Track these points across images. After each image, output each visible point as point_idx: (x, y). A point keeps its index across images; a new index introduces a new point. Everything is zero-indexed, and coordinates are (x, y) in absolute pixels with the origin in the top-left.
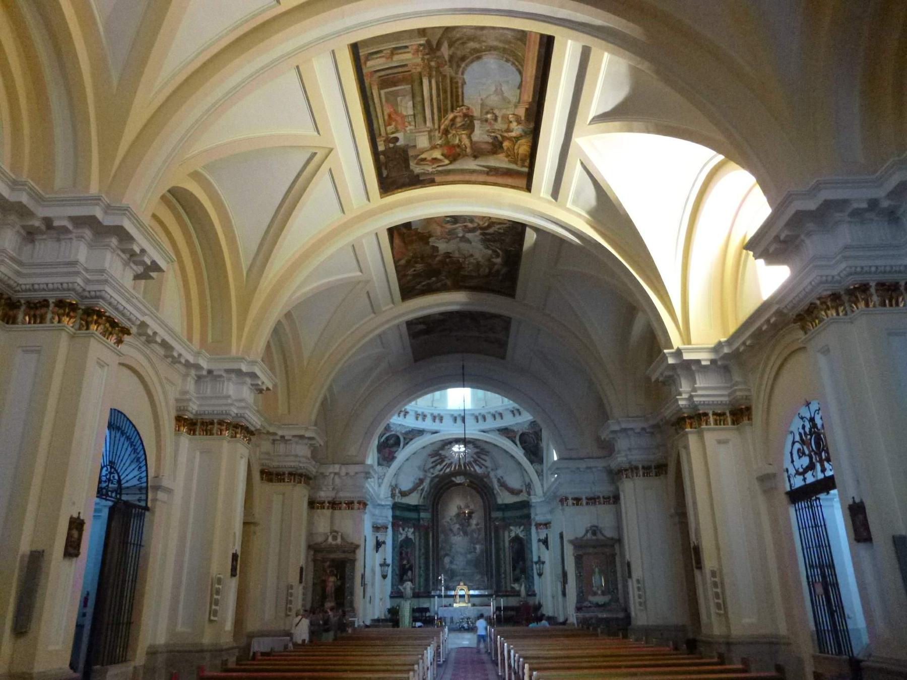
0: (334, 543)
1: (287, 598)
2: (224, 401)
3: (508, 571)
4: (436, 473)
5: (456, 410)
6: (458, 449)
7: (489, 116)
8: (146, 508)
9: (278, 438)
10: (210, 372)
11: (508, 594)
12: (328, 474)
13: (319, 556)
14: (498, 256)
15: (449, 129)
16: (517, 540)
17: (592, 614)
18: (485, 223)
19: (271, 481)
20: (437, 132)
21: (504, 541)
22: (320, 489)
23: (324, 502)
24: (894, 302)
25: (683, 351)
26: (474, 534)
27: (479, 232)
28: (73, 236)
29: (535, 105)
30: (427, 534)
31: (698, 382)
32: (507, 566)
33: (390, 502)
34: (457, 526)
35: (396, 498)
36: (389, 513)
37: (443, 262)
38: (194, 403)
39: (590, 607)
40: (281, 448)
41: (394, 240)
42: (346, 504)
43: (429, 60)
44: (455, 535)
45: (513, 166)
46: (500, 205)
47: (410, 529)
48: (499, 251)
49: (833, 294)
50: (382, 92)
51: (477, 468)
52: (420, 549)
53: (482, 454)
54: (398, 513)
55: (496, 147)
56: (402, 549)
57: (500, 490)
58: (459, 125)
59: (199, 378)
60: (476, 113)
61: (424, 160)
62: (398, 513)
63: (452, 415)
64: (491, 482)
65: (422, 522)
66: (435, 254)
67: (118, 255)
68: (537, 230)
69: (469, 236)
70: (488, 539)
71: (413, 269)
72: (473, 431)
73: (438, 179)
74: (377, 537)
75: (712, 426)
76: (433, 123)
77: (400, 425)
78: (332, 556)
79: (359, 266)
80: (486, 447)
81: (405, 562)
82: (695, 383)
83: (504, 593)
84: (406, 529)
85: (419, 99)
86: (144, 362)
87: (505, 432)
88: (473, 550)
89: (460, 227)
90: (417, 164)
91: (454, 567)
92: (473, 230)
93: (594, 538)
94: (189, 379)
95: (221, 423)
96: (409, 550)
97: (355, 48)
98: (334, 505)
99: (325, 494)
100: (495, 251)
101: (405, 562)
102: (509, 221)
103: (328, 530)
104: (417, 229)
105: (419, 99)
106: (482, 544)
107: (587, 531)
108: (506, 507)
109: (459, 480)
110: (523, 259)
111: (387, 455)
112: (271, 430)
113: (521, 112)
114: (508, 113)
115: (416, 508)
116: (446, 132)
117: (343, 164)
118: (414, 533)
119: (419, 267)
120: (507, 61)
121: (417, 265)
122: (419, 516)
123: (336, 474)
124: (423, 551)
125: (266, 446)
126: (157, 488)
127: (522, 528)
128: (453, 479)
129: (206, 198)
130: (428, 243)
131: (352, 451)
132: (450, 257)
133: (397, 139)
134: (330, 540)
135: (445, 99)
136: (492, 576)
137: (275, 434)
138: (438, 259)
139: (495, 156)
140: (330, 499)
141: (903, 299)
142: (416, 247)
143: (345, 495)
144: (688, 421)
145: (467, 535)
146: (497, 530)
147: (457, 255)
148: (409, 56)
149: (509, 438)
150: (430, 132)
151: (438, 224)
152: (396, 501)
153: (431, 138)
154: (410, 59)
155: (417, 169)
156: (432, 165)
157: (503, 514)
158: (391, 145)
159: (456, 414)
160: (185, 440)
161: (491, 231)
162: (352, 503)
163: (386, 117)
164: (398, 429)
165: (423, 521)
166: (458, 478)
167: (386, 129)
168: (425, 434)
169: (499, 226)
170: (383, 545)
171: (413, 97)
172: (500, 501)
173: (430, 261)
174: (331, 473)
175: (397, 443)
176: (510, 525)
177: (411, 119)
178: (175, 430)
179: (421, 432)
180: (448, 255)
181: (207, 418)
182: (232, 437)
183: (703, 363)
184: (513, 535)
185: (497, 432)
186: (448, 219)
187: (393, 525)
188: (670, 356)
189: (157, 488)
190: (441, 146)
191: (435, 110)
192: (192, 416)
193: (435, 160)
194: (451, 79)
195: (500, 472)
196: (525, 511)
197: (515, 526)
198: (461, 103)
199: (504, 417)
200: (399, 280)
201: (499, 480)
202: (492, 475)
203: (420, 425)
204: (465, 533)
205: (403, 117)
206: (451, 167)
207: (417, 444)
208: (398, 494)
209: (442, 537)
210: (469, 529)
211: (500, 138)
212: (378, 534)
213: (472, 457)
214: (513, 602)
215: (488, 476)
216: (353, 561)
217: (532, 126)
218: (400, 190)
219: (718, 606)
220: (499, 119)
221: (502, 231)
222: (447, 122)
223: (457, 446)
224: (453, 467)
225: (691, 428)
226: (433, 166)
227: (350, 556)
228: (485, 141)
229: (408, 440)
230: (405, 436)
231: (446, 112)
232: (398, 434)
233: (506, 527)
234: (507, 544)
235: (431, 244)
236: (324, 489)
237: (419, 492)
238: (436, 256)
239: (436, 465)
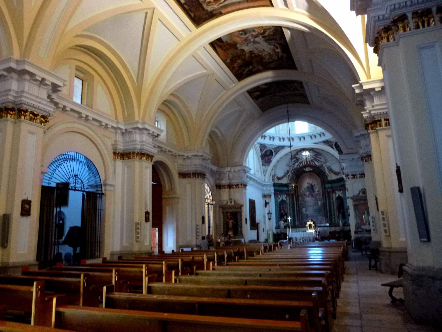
0: (231, 204)
1: (196, 230)
2: (133, 143)
3: (336, 215)
4: (295, 167)
5: (300, 134)
6: (306, 154)
8: (103, 194)
9: (186, 157)
10: (126, 130)
11: (336, 225)
12: (225, 172)
13: (225, 211)
14: (277, 48)
16: (339, 198)
17: (362, 235)
18: (261, 31)
19: (184, 177)
21: (333, 199)
22: (223, 179)
23: (225, 185)
24: (426, 24)
25: (362, 84)
26: (317, 196)
27: (261, 36)
28: (8, 78)
30: (293, 197)
31: (375, 101)
32: (335, 212)
33: (271, 182)
34: (308, 193)
35: (275, 181)
36: (272, 189)
37: (251, 57)
38: (138, 145)
39: (362, 231)
40: (188, 162)
41: (217, 50)
42: (235, 186)
44: (307, 197)
46: (260, 18)
47: (284, 196)
48: (276, 45)
49: (385, 28)
51: (316, 163)
52: (290, 205)
53: (318, 155)
54: (277, 188)
56: (280, 206)
57: (329, 173)
59: (123, 134)
62: (277, 188)
63: (298, 137)
64: (324, 169)
65: (290, 192)
66: (244, 53)
67: (32, 83)
68: (288, 28)
69: (257, 39)
70: (324, 198)
71: (237, 63)
72: (309, 143)
73: (223, 11)
74: (265, 201)
75: (384, 127)
77: (271, 145)
78: (231, 211)
79: (204, 67)
80: (321, 152)
81: (282, 212)
82: (374, 102)
83: (334, 225)
84: (282, 196)
86: (87, 130)
87: (327, 142)
88: (316, 204)
89: (249, 35)
90: (207, 5)
91: (308, 213)
92: (256, 36)
93: (364, 195)
94: (118, 135)
95: (133, 153)
96: (284, 206)
98: (230, 186)
99: (225, 182)
100: (274, 45)
101: (282, 212)
102: (273, 26)
103: (228, 199)
104: (227, 41)
106: (321, 201)
107: (360, 192)
108: (333, 182)
109: (307, 169)
110: (290, 47)
111: (267, 160)
112: (181, 154)
115: (286, 185)
118: (286, 197)
119: (239, 61)
121: (237, 61)
122: (288, 189)
123: (229, 172)
124: (291, 205)
125: (180, 161)
126: (105, 185)
127: (342, 192)
128: (305, 169)
129: (104, 48)
130: (237, 48)
131: (237, 160)
132: (254, 53)
134: (229, 203)
136: (327, 217)
137: (183, 156)
138: (247, 55)
140: (228, 184)
141: (434, 20)
142: (231, 51)
143: (234, 182)
144: (370, 126)
145: (313, 197)
146: (329, 193)
147: (256, 51)
149: (329, 145)
151: (237, 36)
152: (275, 182)
155: (209, 9)
156: (216, 3)
157: (332, 185)
159: (300, 136)
160: (119, 163)
161: (266, 34)
162: (238, 185)
164: (271, 147)
165: (291, 191)
166: (307, 169)
168: (285, 148)
169: (269, 31)
170: (268, 204)
172: (329, 179)
173: (243, 57)
174: (226, 172)
175: (271, 153)
176: (335, 190)
178: (114, 158)
179: (283, 147)
180: (251, 52)
181: (128, 151)
182: (140, 159)
183: (376, 90)
184: (337, 195)
185: (323, 143)
186: (241, 32)
187: (275, 194)
188: (357, 89)
189: (105, 185)
192: (138, 151)
195: (328, 164)
196: (342, 183)
197: (338, 191)
199: (325, 135)
200: (232, 70)
201: (328, 168)
202: (324, 165)
203: (282, 143)
204: (312, 196)
207: (282, 153)
208: (276, 179)
209: (300, 198)
210: (314, 194)
212: (265, 199)
213: (313, 157)
214: (338, 229)
215: (322, 166)
216: (241, 213)
218: (205, 22)
219: (386, 231)
221: (272, 33)
223: (304, 152)
224: (304, 163)
225: (372, 129)
226: (218, 4)
227: (239, 210)
229: (277, 152)
230: (275, 150)
232: (271, 149)
233: (334, 191)
234: (334, 200)
235: (239, 48)
236: (225, 179)
237: (288, 177)
238: (246, 54)
239: (295, 163)
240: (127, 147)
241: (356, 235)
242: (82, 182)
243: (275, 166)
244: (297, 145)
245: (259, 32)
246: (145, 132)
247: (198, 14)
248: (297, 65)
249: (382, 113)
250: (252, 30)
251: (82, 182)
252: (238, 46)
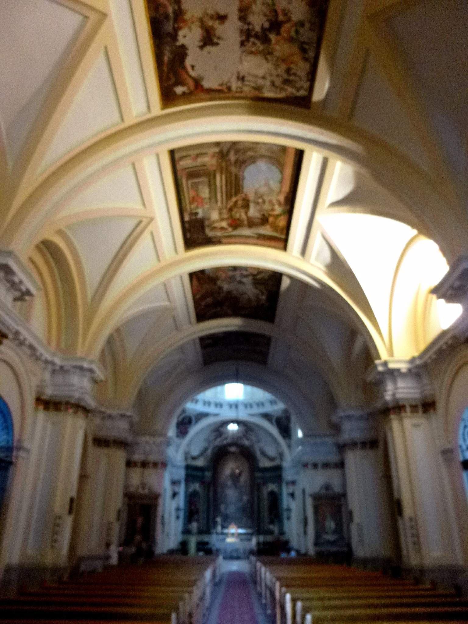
6: (233, 427)
10: (62, 367)
40: (108, 423)
46: (265, 259)
50: (190, 182)
56: (191, 498)
60: (251, 197)
70: (252, 493)
72: (243, 415)
81: (193, 507)
87: (266, 416)
92: (246, 276)
95: (67, 403)
97: (172, 153)
98: (144, 465)
99: (138, 457)
100: (261, 291)
101: (193, 507)
105: (213, 187)
113: (282, 198)
126: (19, 448)
137: (103, 413)
138: (222, 295)
153: (220, 214)
158: (194, 217)
160: (41, 415)
161: (259, 277)
177: (207, 201)
180: (229, 292)
189: (19, 448)
193: (222, 228)
195: (262, 445)
207: (204, 423)
209: (219, 490)
215: (252, 446)
231: (231, 196)
233: (265, 483)
240: (57, 393)
241: (318, 549)
243: (191, 441)
244: (227, 414)
246: (88, 374)
247: (195, 236)
248: (277, 319)
250: (246, 268)
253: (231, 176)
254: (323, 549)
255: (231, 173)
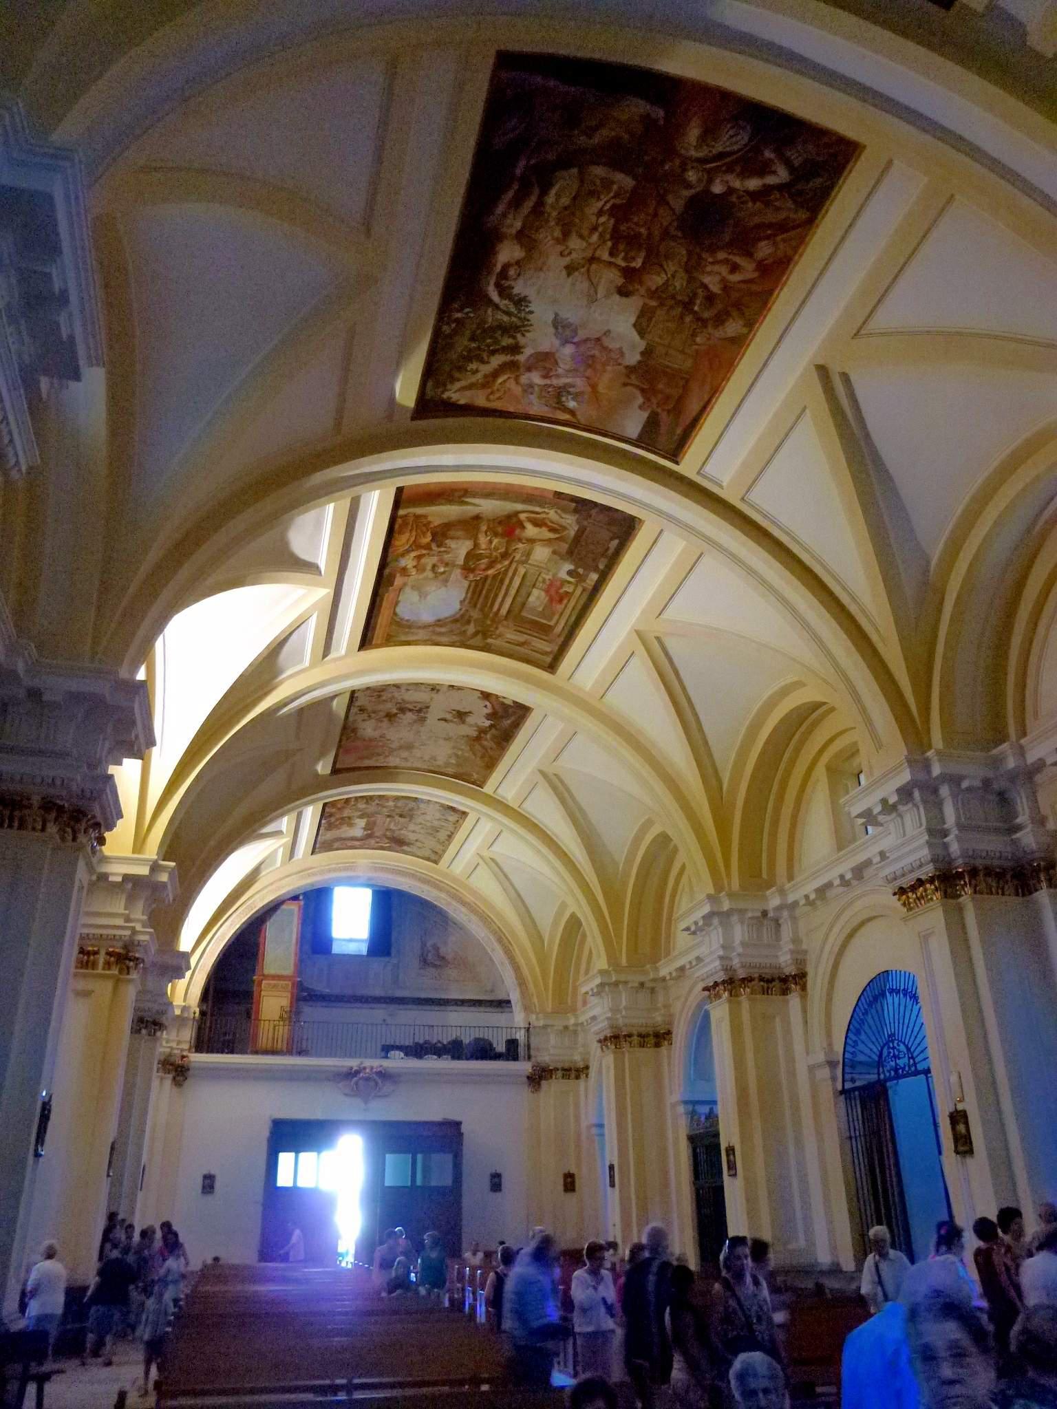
7: (442, 570)
15: (500, 558)
20: (516, 559)
29: (380, 592)
43: (491, 626)
45: (419, 511)
48: (495, 297)
50: (552, 623)
55: (441, 534)
58: (485, 561)
60: (457, 573)
61: (552, 530)
76: (516, 570)
85: (519, 599)
90: (564, 528)
97: (552, 667)
105: (519, 599)
113: (399, 581)
114: (416, 577)
116: (505, 556)
117: (645, 602)
120: (407, 621)
133: (570, 573)
135: (489, 591)
139: (446, 521)
148: (508, 636)
150: (523, 562)
153: (528, 554)
154: (510, 634)
155: (570, 522)
158: (581, 571)
163: (565, 601)
167: (574, 591)
171: (524, 604)
177: (539, 585)
190: (520, 540)
191: (507, 582)
193: (537, 523)
194: (475, 606)
198: (473, 584)
205: (547, 591)
206: (519, 507)
211: (434, 546)
217: (387, 571)
220: (429, 567)
222: (499, 566)
226: (543, 516)
228: (455, 541)
231: (495, 577)
235: (642, 345)
242: (908, 1049)
245: (512, 381)
247: (604, 534)
249: (104, 937)
251: (908, 1049)
252: (633, 358)
253: (484, 605)
254: (875, 1221)
255: (482, 610)
